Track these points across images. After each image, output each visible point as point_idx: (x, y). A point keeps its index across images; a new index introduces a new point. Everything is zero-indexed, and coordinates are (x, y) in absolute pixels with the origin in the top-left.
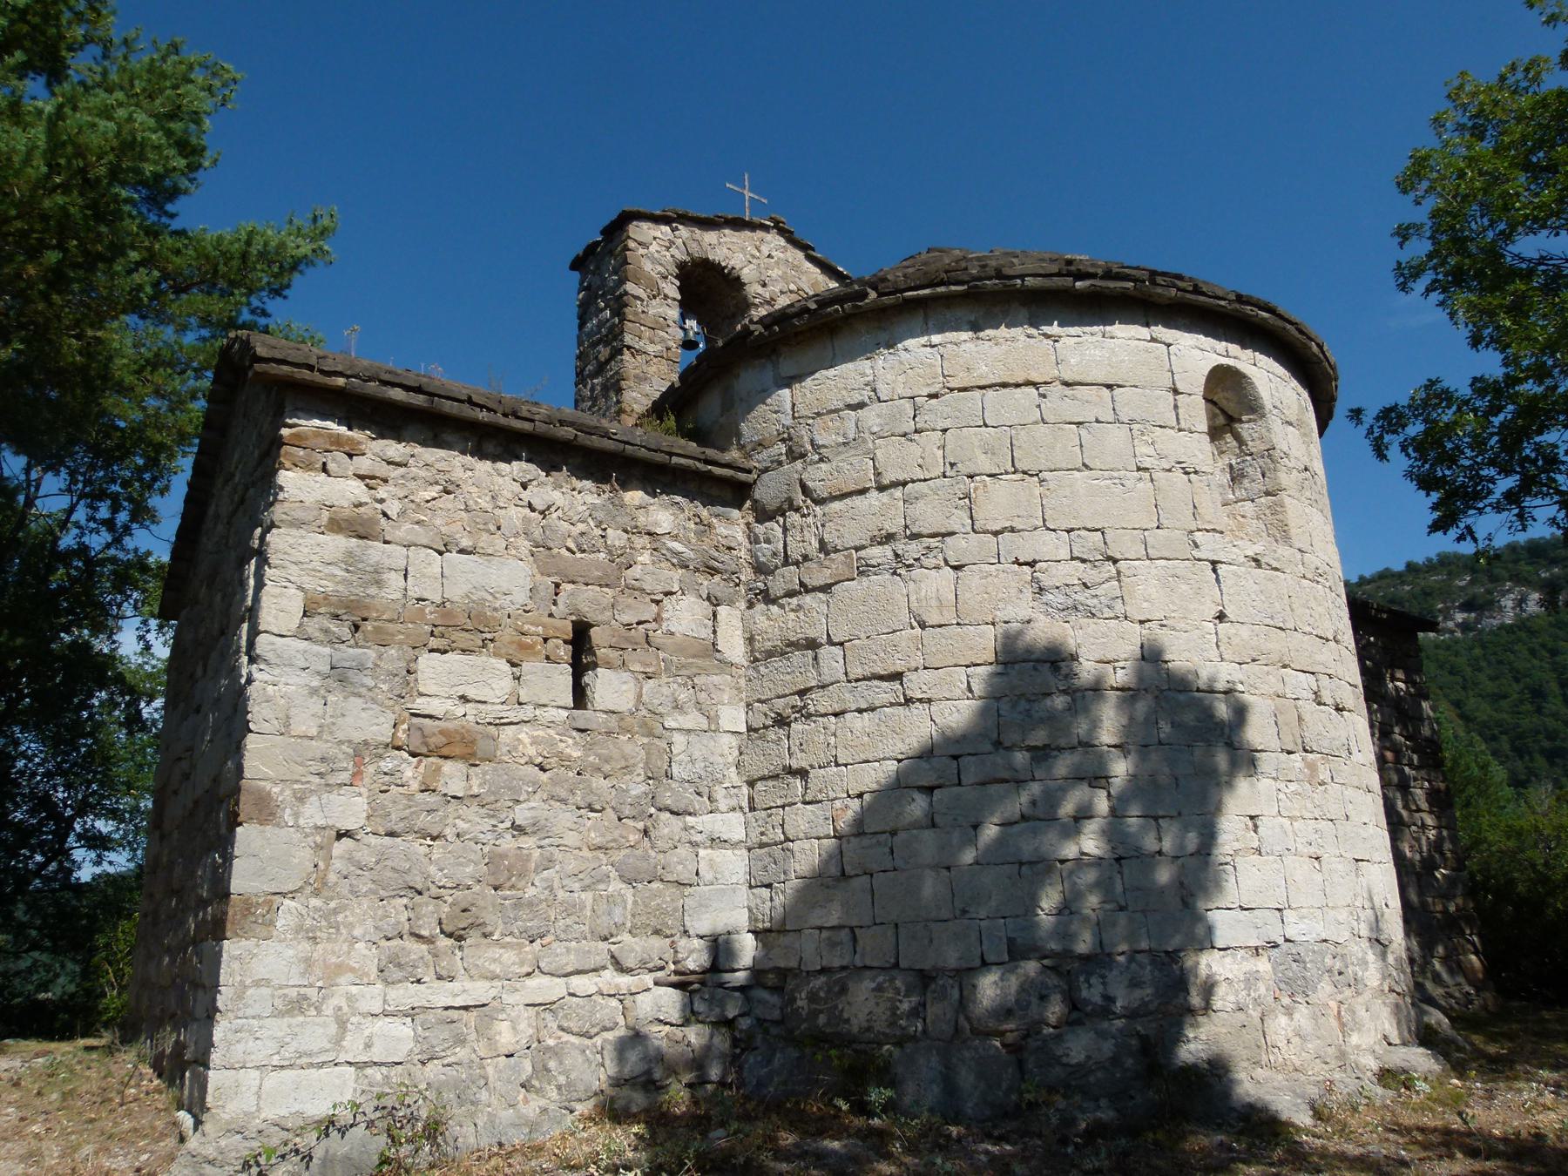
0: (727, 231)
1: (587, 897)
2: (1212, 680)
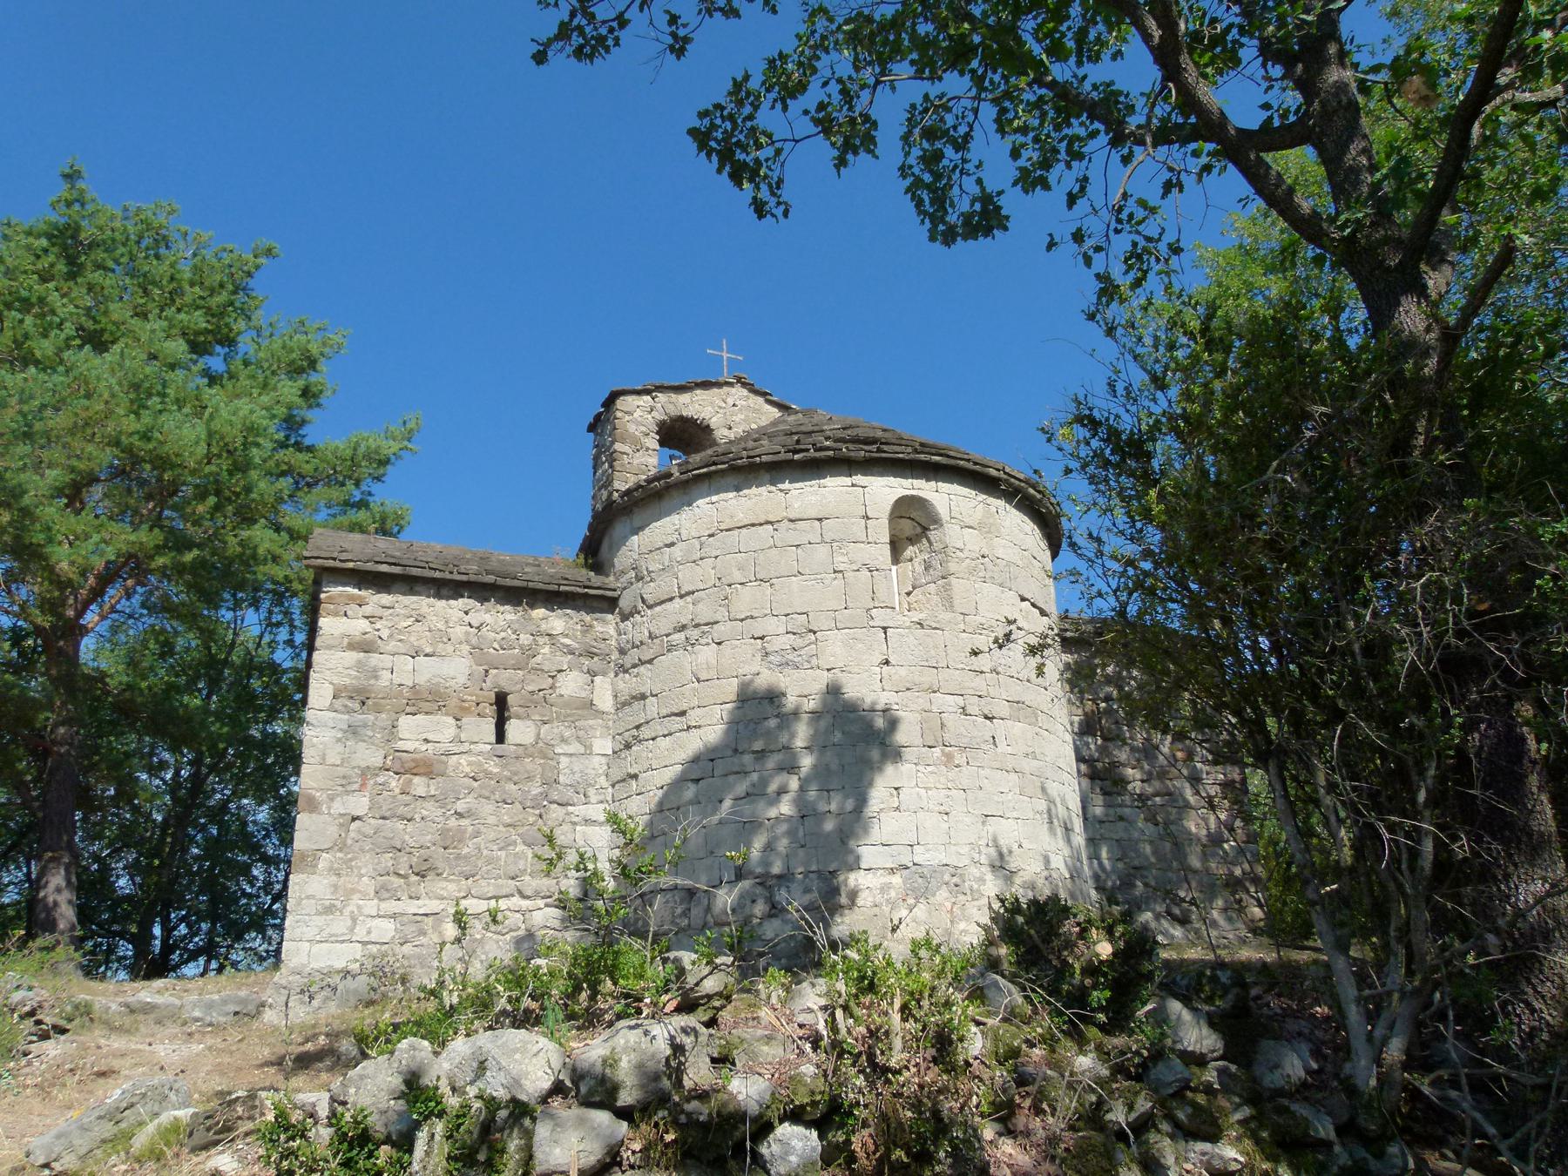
0: (698, 392)
1: (503, 854)
2: (874, 703)
